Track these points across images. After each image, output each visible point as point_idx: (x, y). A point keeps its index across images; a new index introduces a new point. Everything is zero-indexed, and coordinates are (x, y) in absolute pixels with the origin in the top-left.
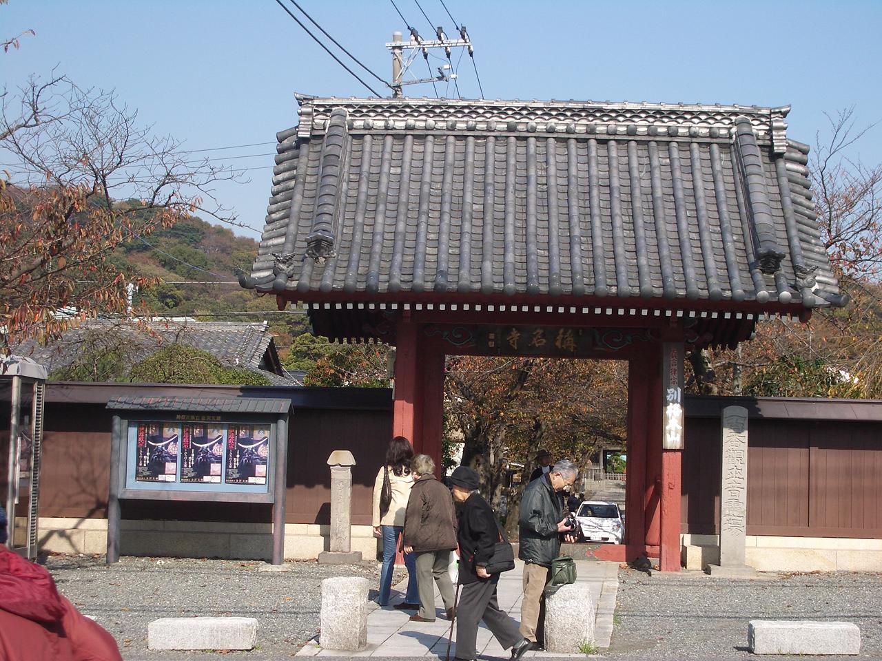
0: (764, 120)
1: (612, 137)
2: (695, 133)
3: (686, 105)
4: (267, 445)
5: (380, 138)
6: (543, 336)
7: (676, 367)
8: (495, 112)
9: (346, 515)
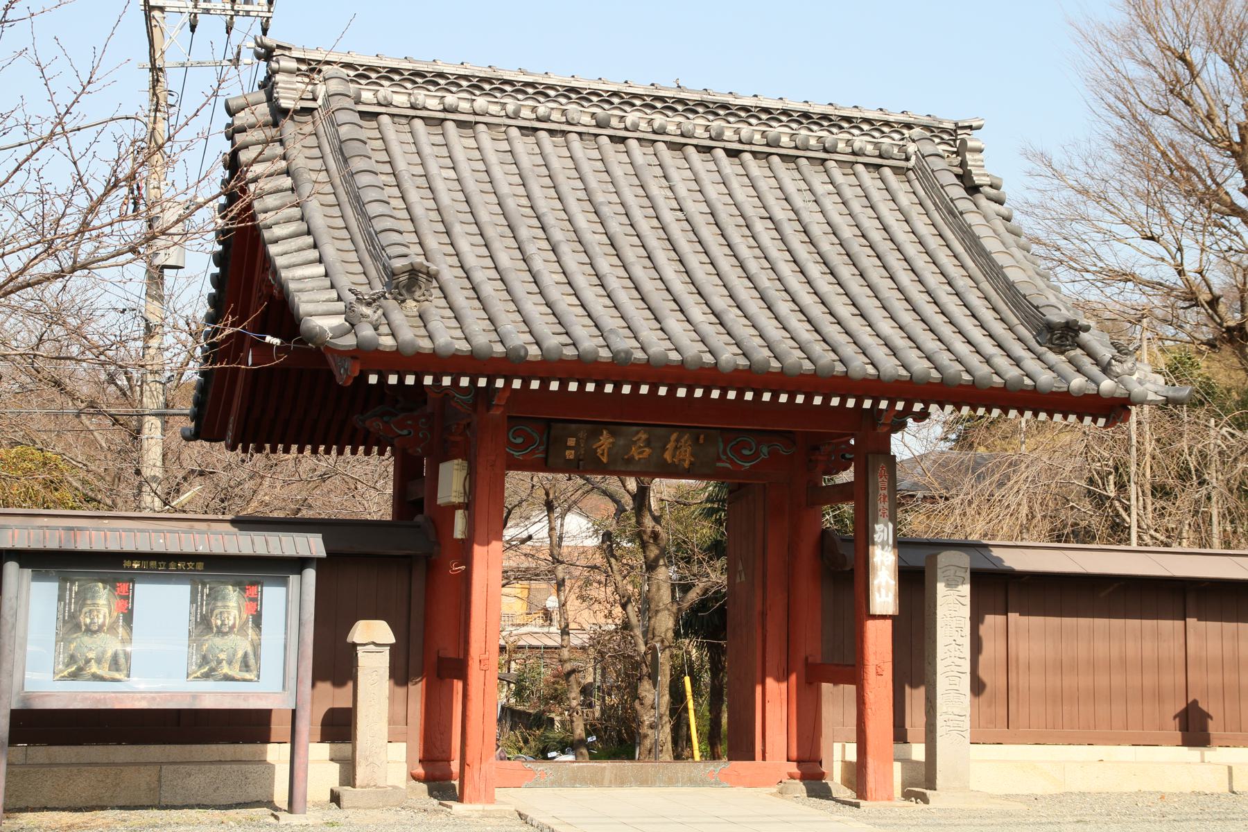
0: (946, 137)
1: (747, 147)
2: (887, 151)
3: (416, 62)
4: (286, 608)
5: (404, 121)
6: (648, 443)
7: (886, 492)
8: (573, 96)
9: (383, 727)
